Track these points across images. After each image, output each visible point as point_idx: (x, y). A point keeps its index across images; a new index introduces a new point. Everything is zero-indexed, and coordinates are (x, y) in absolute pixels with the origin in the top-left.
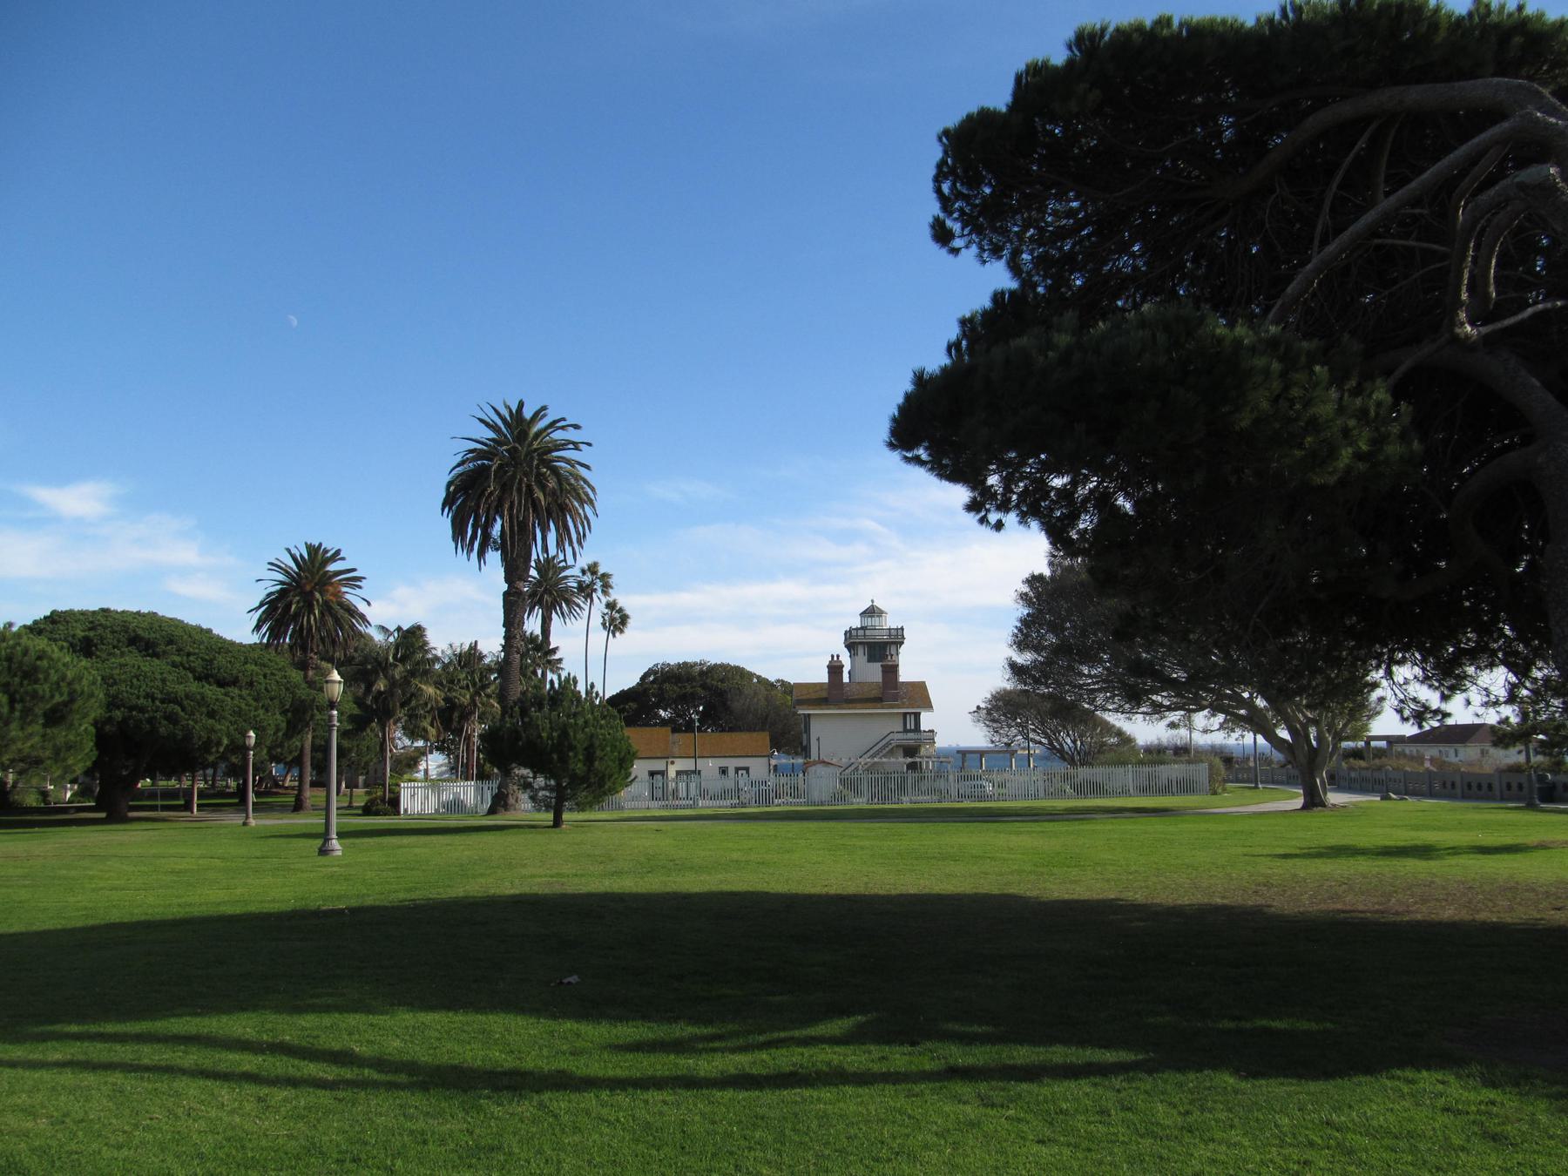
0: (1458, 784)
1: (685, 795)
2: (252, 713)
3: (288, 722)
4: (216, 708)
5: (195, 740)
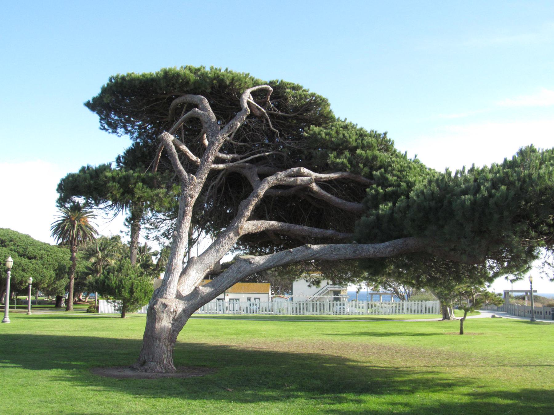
0: (543, 312)
1: (232, 309)
2: (41, 270)
3: (57, 274)
4: (25, 268)
5: (16, 280)
